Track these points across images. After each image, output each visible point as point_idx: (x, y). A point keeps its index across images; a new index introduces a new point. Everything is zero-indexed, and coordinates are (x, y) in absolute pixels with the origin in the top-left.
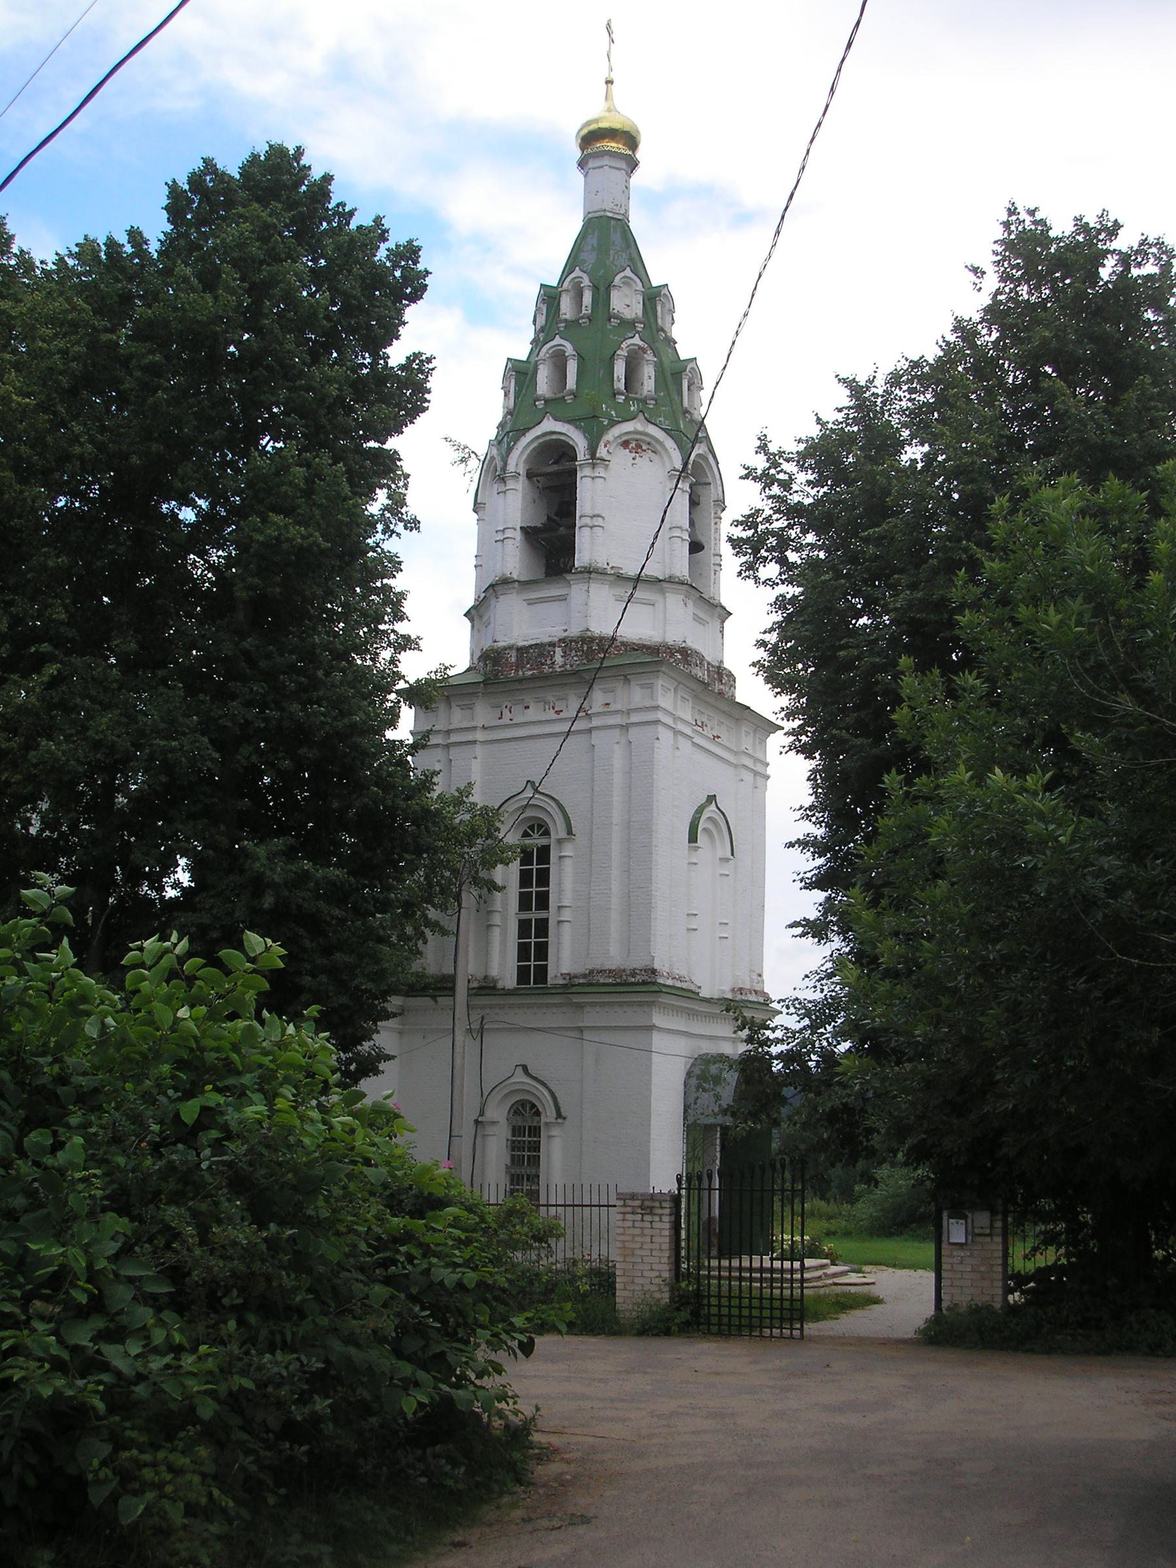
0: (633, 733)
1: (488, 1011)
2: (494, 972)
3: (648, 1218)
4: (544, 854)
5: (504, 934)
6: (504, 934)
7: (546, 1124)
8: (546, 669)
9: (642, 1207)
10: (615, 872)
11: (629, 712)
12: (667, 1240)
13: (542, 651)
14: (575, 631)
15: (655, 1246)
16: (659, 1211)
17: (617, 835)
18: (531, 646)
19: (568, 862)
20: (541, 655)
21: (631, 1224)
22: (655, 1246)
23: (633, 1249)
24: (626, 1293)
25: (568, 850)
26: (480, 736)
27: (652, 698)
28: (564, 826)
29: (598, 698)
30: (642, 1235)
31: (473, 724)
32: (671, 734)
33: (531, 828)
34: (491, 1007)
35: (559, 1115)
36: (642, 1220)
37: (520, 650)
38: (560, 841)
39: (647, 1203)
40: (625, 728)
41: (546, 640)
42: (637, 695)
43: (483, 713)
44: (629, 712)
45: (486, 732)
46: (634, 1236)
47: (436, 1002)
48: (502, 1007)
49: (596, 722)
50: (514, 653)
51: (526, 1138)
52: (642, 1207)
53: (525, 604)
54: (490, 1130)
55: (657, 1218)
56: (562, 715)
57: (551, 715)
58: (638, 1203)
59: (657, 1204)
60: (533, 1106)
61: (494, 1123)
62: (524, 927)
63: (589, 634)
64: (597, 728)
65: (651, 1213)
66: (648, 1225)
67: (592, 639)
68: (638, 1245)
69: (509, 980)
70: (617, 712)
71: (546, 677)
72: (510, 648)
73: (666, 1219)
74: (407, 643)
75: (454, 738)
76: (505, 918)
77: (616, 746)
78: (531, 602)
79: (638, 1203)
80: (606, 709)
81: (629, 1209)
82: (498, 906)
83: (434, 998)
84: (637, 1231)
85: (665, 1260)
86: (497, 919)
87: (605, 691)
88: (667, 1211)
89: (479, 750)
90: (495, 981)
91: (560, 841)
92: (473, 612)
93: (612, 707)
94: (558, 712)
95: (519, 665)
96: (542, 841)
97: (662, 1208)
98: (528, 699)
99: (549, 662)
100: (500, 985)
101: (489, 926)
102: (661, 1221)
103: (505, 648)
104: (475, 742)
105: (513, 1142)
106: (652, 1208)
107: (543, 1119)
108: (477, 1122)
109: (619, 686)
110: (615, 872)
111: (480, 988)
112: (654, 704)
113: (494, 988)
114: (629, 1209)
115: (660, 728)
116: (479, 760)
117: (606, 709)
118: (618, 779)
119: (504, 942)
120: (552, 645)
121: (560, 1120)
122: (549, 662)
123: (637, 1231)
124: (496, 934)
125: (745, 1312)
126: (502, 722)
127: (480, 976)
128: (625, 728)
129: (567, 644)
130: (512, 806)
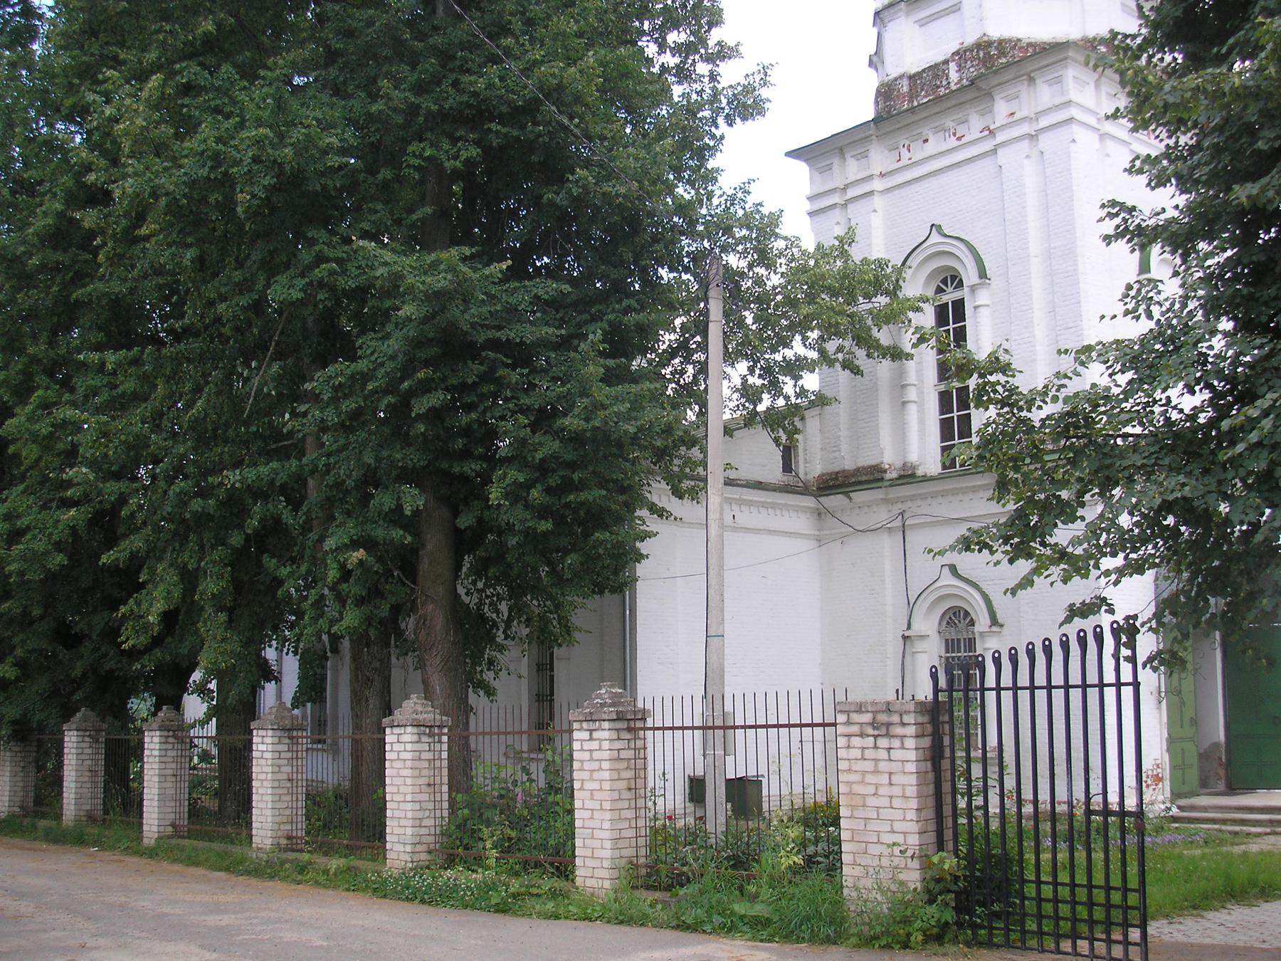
0: (1045, 141)
1: (909, 504)
2: (913, 457)
3: (883, 742)
4: (959, 305)
5: (921, 411)
6: (921, 411)
7: (981, 633)
8: (942, 91)
9: (873, 724)
10: (1039, 315)
11: (1039, 114)
12: (913, 779)
13: (937, 70)
14: (970, 40)
15: (897, 791)
16: (898, 730)
17: (1036, 268)
18: (924, 71)
19: (983, 311)
20: (936, 76)
21: (857, 753)
22: (897, 791)
23: (864, 796)
24: (858, 871)
25: (983, 297)
26: (877, 185)
27: (1062, 93)
28: (975, 269)
29: (1001, 108)
30: (876, 772)
31: (868, 173)
32: (1095, 137)
33: (944, 281)
34: (912, 498)
35: (994, 621)
36: (876, 747)
37: (912, 78)
38: (973, 289)
39: (882, 718)
40: (1033, 137)
41: (940, 59)
42: (1044, 94)
43: (879, 158)
44: (1039, 114)
45: (884, 180)
46: (864, 773)
47: (850, 499)
48: (924, 497)
49: (1000, 137)
50: (905, 82)
51: (962, 654)
52: (873, 724)
53: (916, 26)
54: (920, 646)
55: (896, 743)
56: (964, 140)
57: (953, 142)
58: (867, 718)
59: (896, 719)
60: (967, 613)
61: (922, 637)
62: (945, 399)
63: (986, 38)
64: (1002, 144)
65: (888, 735)
66: (883, 754)
67: (989, 44)
68: (871, 790)
69: (931, 463)
70: (1023, 119)
71: (939, 99)
72: (901, 77)
73: (911, 743)
74: (724, 53)
75: (852, 193)
76: (921, 393)
77: (1026, 161)
78: (923, 23)
79: (867, 718)
80: (1011, 120)
81: (855, 729)
82: (912, 378)
83: (846, 494)
84: (869, 766)
85: (912, 815)
86: (912, 394)
87: (1009, 99)
88: (911, 730)
89: (878, 201)
90: (914, 468)
91: (973, 289)
92: (875, 59)
93: (1016, 117)
94: (959, 139)
95: (912, 94)
96: (956, 295)
97: (903, 724)
98: (926, 131)
99: (944, 83)
100: (920, 472)
101: (904, 403)
102: (903, 747)
103: (896, 79)
104: (872, 193)
105: (947, 658)
106: (888, 725)
107: (977, 628)
108: (905, 638)
109: (1023, 88)
110: (1039, 315)
111: (901, 477)
112: (1064, 99)
113: (913, 475)
114: (855, 729)
115: (1076, 130)
116: (880, 213)
117: (1011, 120)
118: (1032, 200)
119: (922, 422)
120: (946, 62)
121: (994, 629)
122: (944, 83)
123: (869, 766)
124: (912, 410)
125: (1064, 910)
126: (901, 164)
127: (899, 464)
128: (1033, 137)
129: (961, 56)
130: (914, 262)
